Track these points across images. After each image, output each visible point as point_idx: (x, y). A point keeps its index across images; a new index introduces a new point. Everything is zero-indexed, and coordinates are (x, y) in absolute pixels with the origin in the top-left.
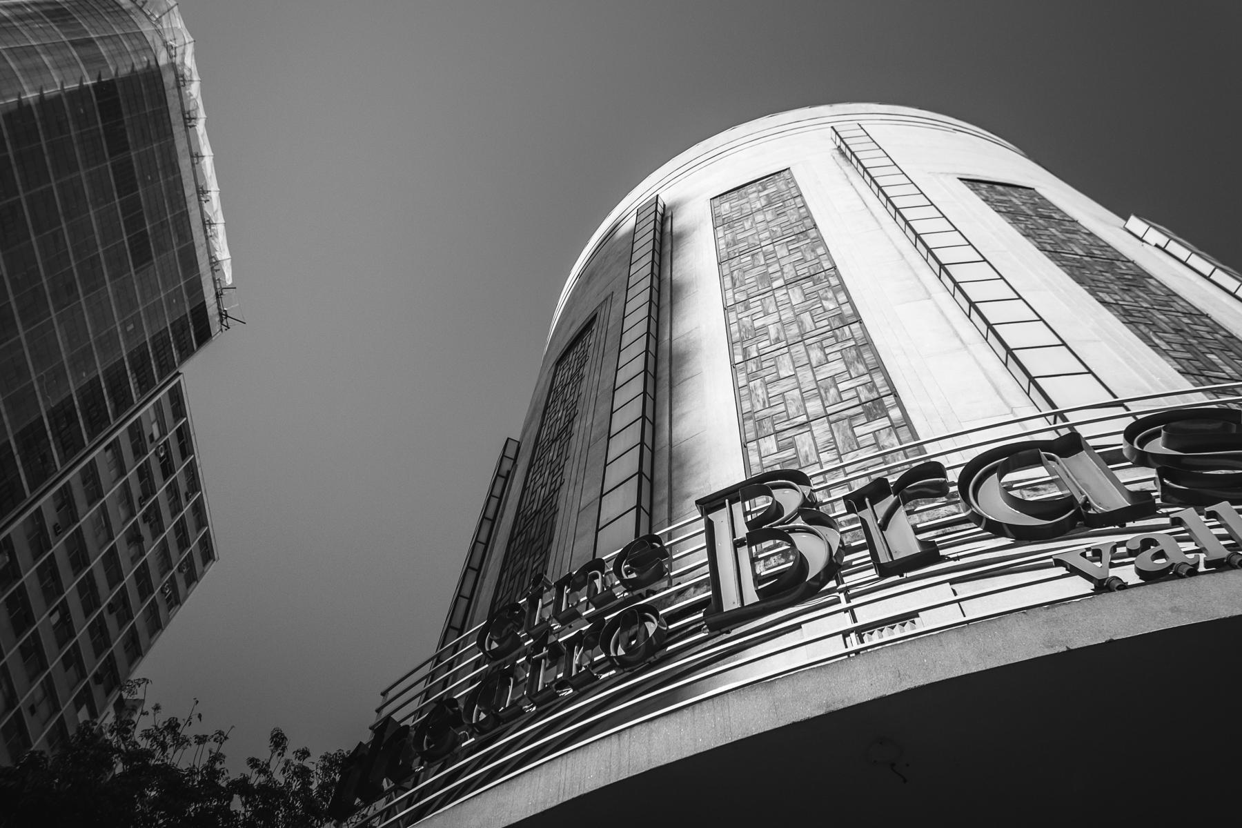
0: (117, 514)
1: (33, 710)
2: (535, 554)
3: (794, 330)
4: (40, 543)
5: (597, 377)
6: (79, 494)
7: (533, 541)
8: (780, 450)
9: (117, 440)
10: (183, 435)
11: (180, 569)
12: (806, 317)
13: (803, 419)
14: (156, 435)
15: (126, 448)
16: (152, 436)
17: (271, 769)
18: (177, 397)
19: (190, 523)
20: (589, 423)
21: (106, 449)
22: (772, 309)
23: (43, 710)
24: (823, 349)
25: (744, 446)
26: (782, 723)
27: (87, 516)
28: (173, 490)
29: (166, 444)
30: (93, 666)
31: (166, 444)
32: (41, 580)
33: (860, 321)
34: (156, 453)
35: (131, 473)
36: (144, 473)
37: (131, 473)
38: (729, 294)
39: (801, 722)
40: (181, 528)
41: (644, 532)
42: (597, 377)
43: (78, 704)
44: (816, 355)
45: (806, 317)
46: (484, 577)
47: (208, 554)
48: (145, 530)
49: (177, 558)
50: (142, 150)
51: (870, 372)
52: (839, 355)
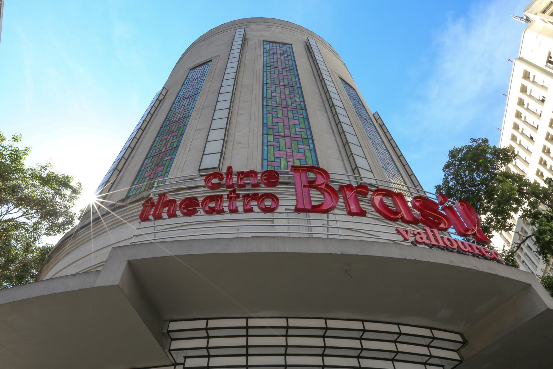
2: (174, 137)
5: (209, 84)
7: (173, 132)
8: (274, 142)
12: (289, 100)
13: (283, 134)
20: (204, 99)
22: (278, 91)
24: (293, 114)
25: (263, 135)
26: (328, 252)
33: (306, 110)
38: (265, 79)
39: (409, 260)
42: (209, 84)
44: (290, 115)
45: (289, 100)
46: (146, 134)
50: (103, 221)
51: (306, 129)
52: (297, 118)
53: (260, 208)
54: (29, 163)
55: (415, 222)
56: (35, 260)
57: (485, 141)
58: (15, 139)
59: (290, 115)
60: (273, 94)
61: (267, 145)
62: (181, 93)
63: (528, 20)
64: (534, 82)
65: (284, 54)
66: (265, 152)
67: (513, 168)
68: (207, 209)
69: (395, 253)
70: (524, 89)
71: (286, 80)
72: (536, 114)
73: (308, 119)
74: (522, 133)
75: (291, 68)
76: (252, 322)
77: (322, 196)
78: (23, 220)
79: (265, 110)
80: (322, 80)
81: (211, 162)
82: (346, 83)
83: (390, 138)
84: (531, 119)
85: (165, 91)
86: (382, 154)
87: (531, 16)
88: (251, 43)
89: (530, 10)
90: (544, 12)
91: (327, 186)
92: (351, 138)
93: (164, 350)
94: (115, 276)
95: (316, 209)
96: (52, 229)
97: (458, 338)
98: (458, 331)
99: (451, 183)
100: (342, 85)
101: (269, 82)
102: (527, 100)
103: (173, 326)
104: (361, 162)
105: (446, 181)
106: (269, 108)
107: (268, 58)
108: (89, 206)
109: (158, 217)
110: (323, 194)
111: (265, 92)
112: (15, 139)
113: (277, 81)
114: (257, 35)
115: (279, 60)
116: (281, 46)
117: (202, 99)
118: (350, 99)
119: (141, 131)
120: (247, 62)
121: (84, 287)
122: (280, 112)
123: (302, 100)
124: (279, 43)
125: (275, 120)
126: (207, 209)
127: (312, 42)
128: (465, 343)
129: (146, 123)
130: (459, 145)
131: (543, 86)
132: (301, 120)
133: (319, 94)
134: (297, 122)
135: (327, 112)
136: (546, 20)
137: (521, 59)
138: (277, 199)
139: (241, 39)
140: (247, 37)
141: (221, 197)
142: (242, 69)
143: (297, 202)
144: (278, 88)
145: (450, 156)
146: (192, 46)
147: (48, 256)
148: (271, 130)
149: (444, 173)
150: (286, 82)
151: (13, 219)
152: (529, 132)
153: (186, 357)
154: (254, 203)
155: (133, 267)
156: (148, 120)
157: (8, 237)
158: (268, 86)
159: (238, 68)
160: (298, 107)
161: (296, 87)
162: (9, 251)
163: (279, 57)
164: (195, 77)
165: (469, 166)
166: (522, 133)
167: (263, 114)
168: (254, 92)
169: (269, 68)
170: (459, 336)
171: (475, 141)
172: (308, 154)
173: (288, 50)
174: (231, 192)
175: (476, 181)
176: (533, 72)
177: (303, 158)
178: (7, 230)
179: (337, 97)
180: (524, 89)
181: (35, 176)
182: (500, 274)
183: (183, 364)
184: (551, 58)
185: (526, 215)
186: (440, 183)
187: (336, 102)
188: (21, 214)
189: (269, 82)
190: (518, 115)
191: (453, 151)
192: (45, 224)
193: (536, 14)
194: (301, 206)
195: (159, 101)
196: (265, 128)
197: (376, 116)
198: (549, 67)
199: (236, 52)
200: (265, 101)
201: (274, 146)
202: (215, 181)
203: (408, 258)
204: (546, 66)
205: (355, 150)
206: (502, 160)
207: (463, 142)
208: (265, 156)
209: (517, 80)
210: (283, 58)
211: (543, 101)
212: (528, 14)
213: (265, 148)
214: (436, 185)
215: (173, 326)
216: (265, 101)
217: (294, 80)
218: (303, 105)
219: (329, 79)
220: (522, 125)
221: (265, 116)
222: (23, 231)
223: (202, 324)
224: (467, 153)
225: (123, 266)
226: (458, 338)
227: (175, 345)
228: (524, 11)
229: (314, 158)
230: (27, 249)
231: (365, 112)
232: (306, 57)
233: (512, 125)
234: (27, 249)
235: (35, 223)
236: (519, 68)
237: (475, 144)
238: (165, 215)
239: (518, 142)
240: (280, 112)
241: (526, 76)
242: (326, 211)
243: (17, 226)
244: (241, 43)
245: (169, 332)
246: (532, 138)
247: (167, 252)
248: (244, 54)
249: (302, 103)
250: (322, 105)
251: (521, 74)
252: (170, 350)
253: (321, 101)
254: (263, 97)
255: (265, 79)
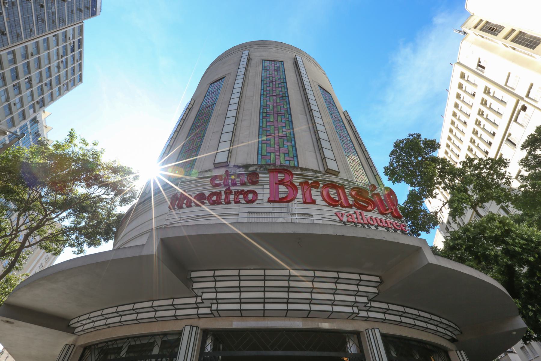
0: (54, 57)
1: (15, 104)
3: (275, 110)
4: (26, 56)
6: (42, 46)
9: (57, 34)
10: (80, 42)
11: (70, 81)
12: (279, 107)
14: (71, 38)
15: (61, 38)
16: (69, 38)
17: (308, 159)
18: (81, 29)
19: (77, 69)
21: (54, 36)
22: (272, 101)
23: (18, 105)
27: (43, 54)
28: (73, 57)
29: (74, 42)
30: (37, 98)
31: (74, 42)
32: (24, 68)
33: (291, 115)
34: (70, 44)
35: (60, 47)
36: (65, 47)
37: (60, 47)
38: (262, 91)
40: (74, 69)
41: (326, 169)
43: (30, 107)
47: (81, 80)
48: (62, 66)
49: (71, 78)
53: (245, 201)
54: (104, 159)
55: (350, 206)
56: (114, 222)
57: (419, 136)
58: (95, 144)
59: (279, 119)
60: (268, 103)
61: (262, 143)
62: (204, 103)
63: (465, 33)
64: (468, 81)
65: (277, 70)
66: (260, 149)
67: (440, 154)
68: (211, 202)
69: (330, 232)
70: (460, 86)
71: (277, 91)
72: (469, 105)
73: (292, 121)
74: (459, 119)
75: (282, 81)
76: (243, 272)
77: (287, 190)
78: (104, 196)
79: (261, 116)
80: (304, 90)
81: (222, 158)
82: (324, 89)
83: (355, 131)
84: (465, 108)
85: (193, 101)
86: (347, 144)
87: (467, 30)
88: (253, 62)
89: (465, 26)
90: (475, 27)
91: (291, 183)
92: (322, 135)
93: (189, 288)
94: (154, 248)
95: (282, 200)
96: (124, 201)
97: (377, 279)
98: (378, 275)
99: (395, 165)
100: (319, 92)
101: (265, 93)
102: (463, 94)
103: (194, 274)
104: (328, 154)
105: (391, 164)
106: (264, 115)
107: (265, 74)
108: (148, 185)
109: (180, 207)
110: (287, 189)
111: (262, 102)
112: (95, 144)
113: (271, 93)
114: (258, 55)
115: (273, 75)
116: (275, 63)
117: (218, 109)
118: (326, 102)
119: (182, 121)
120: (250, 78)
121: (135, 255)
122: (272, 117)
123: (288, 106)
124: (274, 61)
125: (268, 124)
126: (211, 202)
127: (299, 59)
128: (381, 282)
129: (185, 115)
130: (401, 138)
131: (474, 84)
132: (287, 122)
133: (301, 101)
134: (284, 125)
135: (306, 115)
136: (477, 34)
137: (459, 63)
138: (256, 194)
139: (246, 60)
140: (251, 57)
141: (220, 193)
142: (246, 84)
143: (270, 195)
144: (271, 98)
145: (394, 146)
146: (212, 64)
147: (121, 220)
148: (265, 132)
149: (390, 158)
150: (278, 93)
151: (99, 196)
152: (463, 118)
153: (203, 293)
154: (241, 196)
155: (165, 243)
156: (181, 124)
157: (96, 207)
158: (264, 96)
159: (243, 83)
160: (285, 113)
161: (285, 97)
162: (98, 215)
163: (273, 72)
164: (213, 90)
165: (409, 152)
166: (459, 119)
167: (260, 119)
168: (254, 102)
169: (265, 82)
170: (378, 278)
171: (412, 135)
172: (290, 149)
173: (281, 66)
174: (226, 190)
175: (413, 163)
176: (467, 73)
177: (287, 152)
178: (95, 203)
179: (315, 103)
180: (460, 86)
181: (108, 168)
182: (400, 242)
183: (201, 296)
184: (480, 62)
185: (446, 187)
186: (387, 165)
187: (313, 107)
188: (103, 191)
189: (265, 93)
190: (456, 106)
191: (396, 142)
192: (118, 199)
193: (470, 29)
194: (272, 199)
195: (189, 109)
196: (261, 130)
197: (346, 114)
198: (478, 69)
199: (242, 71)
200: (262, 109)
201: (266, 144)
202: (217, 182)
203: (338, 234)
204: (477, 68)
205: (324, 144)
206: (431, 148)
207: (403, 136)
208: (260, 152)
209: (456, 80)
210: (276, 73)
211: (474, 95)
212: (463, 29)
213: (260, 145)
214: (384, 166)
215: (194, 274)
216: (262, 109)
217: (283, 91)
218: (289, 111)
219: (310, 88)
220: (458, 113)
221: (261, 121)
222: (105, 203)
223: (211, 273)
224: (406, 144)
225: (159, 239)
226: (377, 279)
227: (196, 285)
228: (462, 26)
229: (294, 152)
230: (109, 214)
231: (336, 112)
232: (293, 70)
233: (452, 113)
234: (109, 214)
235: (112, 198)
236: (457, 70)
237: (411, 138)
238: (184, 206)
239: (456, 126)
240: (272, 117)
241: (463, 76)
242: (289, 202)
243: (102, 200)
244: (246, 62)
245: (191, 278)
246: (465, 123)
247: (184, 233)
248: (248, 72)
249: (289, 109)
250: (303, 109)
251: (459, 75)
252: (193, 289)
253: (302, 106)
254: (260, 106)
255: (262, 91)
